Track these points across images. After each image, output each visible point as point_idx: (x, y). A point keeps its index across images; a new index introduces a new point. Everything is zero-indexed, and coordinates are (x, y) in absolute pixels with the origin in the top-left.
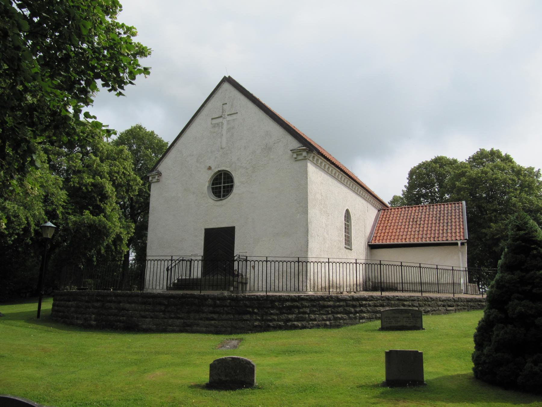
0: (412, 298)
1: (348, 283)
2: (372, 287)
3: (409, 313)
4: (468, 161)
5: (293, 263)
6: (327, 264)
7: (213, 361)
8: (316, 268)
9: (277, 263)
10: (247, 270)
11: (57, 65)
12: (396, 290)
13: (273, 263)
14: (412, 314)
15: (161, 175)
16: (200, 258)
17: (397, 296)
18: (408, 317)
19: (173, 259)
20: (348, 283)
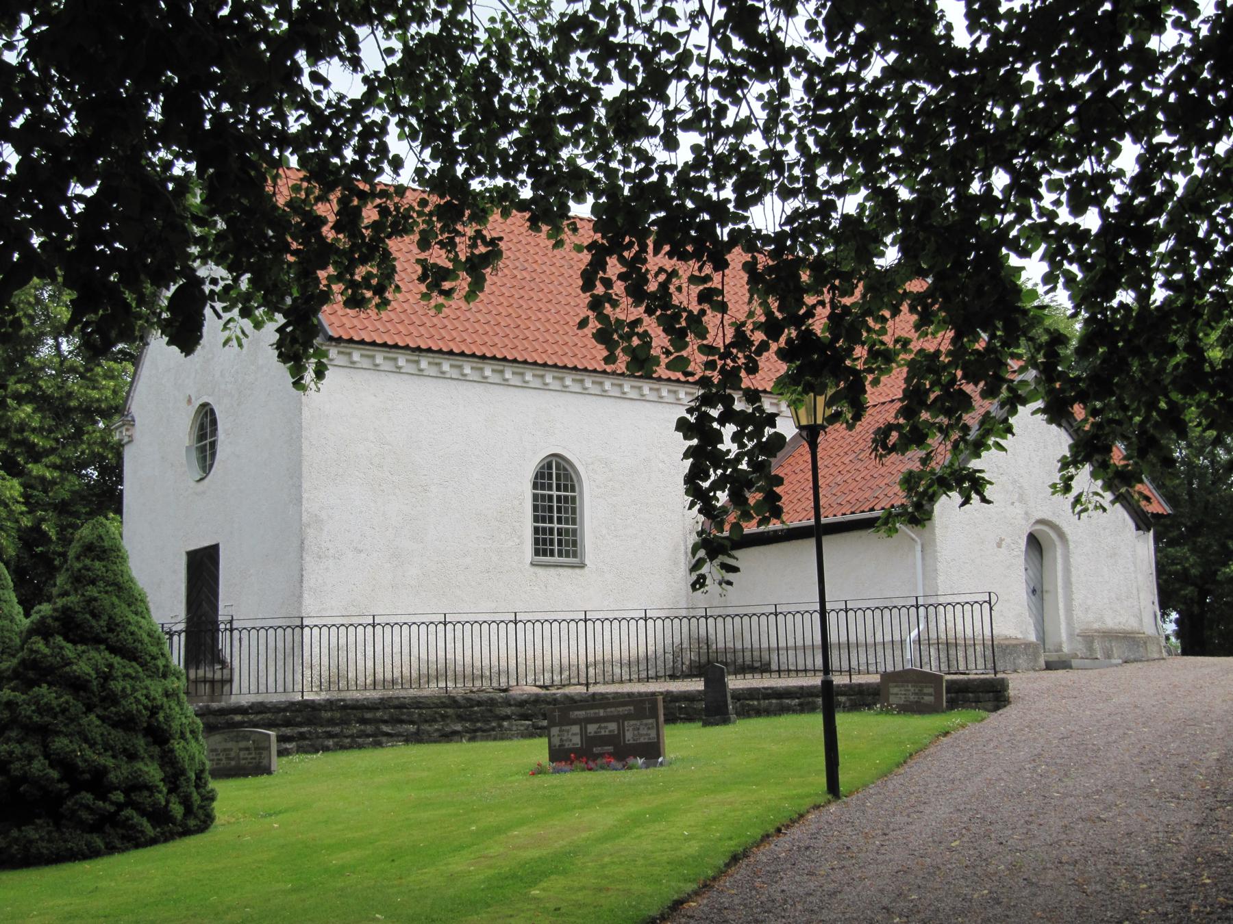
0: (396, 702)
1: (548, 663)
2: (690, 667)
3: (248, 740)
4: (346, 289)
5: (976, 606)
6: (913, 610)
7: (217, 813)
8: (432, 638)
9: (414, 627)
10: (234, 650)
11: (1056, 66)
12: (765, 669)
13: (253, 632)
14: (254, 741)
15: (133, 425)
16: (182, 626)
17: (398, 698)
18: (247, 749)
19: (518, 619)
20: (548, 663)
